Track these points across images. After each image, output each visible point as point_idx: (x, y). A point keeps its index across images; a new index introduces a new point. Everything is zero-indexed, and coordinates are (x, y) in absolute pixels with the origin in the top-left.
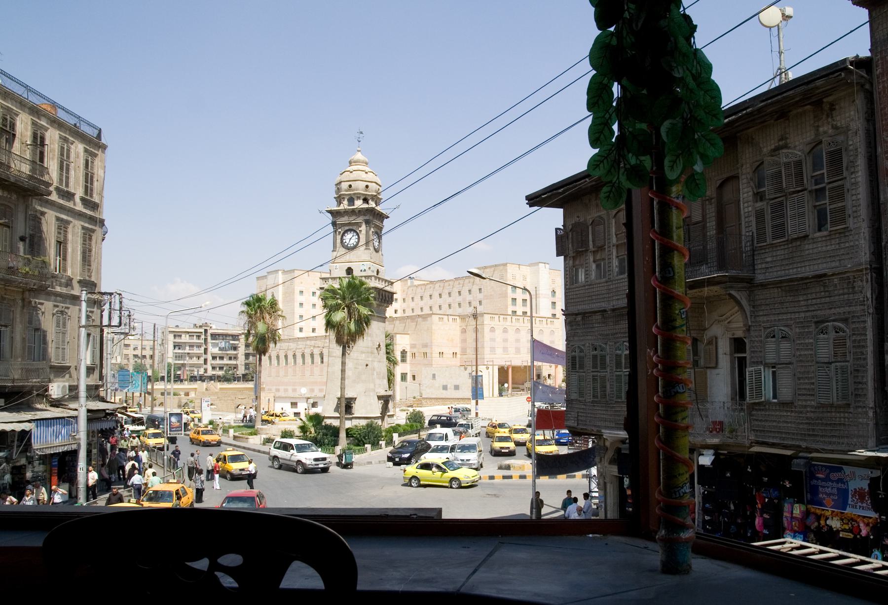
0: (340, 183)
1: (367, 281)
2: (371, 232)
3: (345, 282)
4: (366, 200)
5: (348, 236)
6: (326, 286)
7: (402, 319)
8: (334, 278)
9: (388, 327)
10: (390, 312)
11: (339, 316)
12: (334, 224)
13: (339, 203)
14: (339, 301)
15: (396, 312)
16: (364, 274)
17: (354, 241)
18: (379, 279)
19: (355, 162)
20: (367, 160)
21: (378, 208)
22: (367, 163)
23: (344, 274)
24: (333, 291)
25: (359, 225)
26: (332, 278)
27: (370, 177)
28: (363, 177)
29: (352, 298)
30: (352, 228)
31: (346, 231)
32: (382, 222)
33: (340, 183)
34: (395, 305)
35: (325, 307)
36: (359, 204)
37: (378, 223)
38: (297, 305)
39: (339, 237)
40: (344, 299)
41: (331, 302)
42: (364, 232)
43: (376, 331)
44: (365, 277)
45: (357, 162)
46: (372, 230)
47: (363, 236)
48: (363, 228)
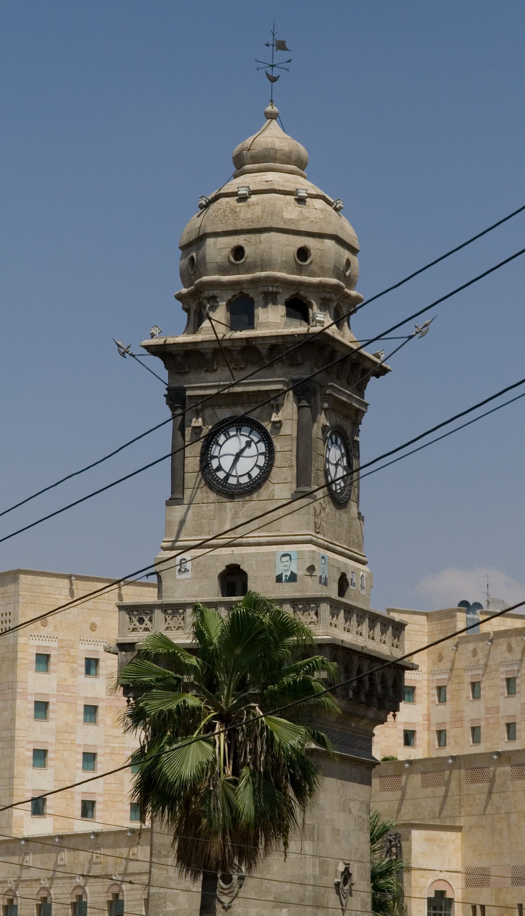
0: (201, 239)
1: (304, 619)
2: (316, 430)
3: (218, 622)
4: (298, 308)
5: (230, 445)
6: (140, 637)
7: (431, 768)
8: (174, 609)
9: (382, 800)
10: (386, 740)
11: (188, 760)
12: (176, 398)
13: (197, 318)
14: (192, 700)
15: (409, 738)
16: (288, 591)
17: (248, 466)
18: (349, 610)
19: (257, 159)
20: (302, 150)
21: (347, 337)
22: (301, 164)
23: (211, 592)
24: (168, 657)
25: (271, 401)
26: (165, 608)
27: (317, 214)
28: (287, 209)
29: (242, 686)
30: (248, 416)
31: (222, 428)
32: (360, 389)
33: (201, 239)
34: (408, 714)
35: (137, 716)
36: (272, 321)
37: (345, 394)
38: (25, 707)
39: (193, 452)
40: (209, 686)
41: (158, 704)
42: (289, 429)
43: (334, 817)
44: (294, 602)
45: (267, 159)
46: (323, 419)
47: (285, 447)
48: (288, 413)
